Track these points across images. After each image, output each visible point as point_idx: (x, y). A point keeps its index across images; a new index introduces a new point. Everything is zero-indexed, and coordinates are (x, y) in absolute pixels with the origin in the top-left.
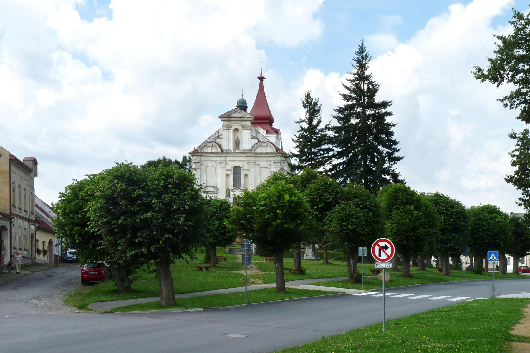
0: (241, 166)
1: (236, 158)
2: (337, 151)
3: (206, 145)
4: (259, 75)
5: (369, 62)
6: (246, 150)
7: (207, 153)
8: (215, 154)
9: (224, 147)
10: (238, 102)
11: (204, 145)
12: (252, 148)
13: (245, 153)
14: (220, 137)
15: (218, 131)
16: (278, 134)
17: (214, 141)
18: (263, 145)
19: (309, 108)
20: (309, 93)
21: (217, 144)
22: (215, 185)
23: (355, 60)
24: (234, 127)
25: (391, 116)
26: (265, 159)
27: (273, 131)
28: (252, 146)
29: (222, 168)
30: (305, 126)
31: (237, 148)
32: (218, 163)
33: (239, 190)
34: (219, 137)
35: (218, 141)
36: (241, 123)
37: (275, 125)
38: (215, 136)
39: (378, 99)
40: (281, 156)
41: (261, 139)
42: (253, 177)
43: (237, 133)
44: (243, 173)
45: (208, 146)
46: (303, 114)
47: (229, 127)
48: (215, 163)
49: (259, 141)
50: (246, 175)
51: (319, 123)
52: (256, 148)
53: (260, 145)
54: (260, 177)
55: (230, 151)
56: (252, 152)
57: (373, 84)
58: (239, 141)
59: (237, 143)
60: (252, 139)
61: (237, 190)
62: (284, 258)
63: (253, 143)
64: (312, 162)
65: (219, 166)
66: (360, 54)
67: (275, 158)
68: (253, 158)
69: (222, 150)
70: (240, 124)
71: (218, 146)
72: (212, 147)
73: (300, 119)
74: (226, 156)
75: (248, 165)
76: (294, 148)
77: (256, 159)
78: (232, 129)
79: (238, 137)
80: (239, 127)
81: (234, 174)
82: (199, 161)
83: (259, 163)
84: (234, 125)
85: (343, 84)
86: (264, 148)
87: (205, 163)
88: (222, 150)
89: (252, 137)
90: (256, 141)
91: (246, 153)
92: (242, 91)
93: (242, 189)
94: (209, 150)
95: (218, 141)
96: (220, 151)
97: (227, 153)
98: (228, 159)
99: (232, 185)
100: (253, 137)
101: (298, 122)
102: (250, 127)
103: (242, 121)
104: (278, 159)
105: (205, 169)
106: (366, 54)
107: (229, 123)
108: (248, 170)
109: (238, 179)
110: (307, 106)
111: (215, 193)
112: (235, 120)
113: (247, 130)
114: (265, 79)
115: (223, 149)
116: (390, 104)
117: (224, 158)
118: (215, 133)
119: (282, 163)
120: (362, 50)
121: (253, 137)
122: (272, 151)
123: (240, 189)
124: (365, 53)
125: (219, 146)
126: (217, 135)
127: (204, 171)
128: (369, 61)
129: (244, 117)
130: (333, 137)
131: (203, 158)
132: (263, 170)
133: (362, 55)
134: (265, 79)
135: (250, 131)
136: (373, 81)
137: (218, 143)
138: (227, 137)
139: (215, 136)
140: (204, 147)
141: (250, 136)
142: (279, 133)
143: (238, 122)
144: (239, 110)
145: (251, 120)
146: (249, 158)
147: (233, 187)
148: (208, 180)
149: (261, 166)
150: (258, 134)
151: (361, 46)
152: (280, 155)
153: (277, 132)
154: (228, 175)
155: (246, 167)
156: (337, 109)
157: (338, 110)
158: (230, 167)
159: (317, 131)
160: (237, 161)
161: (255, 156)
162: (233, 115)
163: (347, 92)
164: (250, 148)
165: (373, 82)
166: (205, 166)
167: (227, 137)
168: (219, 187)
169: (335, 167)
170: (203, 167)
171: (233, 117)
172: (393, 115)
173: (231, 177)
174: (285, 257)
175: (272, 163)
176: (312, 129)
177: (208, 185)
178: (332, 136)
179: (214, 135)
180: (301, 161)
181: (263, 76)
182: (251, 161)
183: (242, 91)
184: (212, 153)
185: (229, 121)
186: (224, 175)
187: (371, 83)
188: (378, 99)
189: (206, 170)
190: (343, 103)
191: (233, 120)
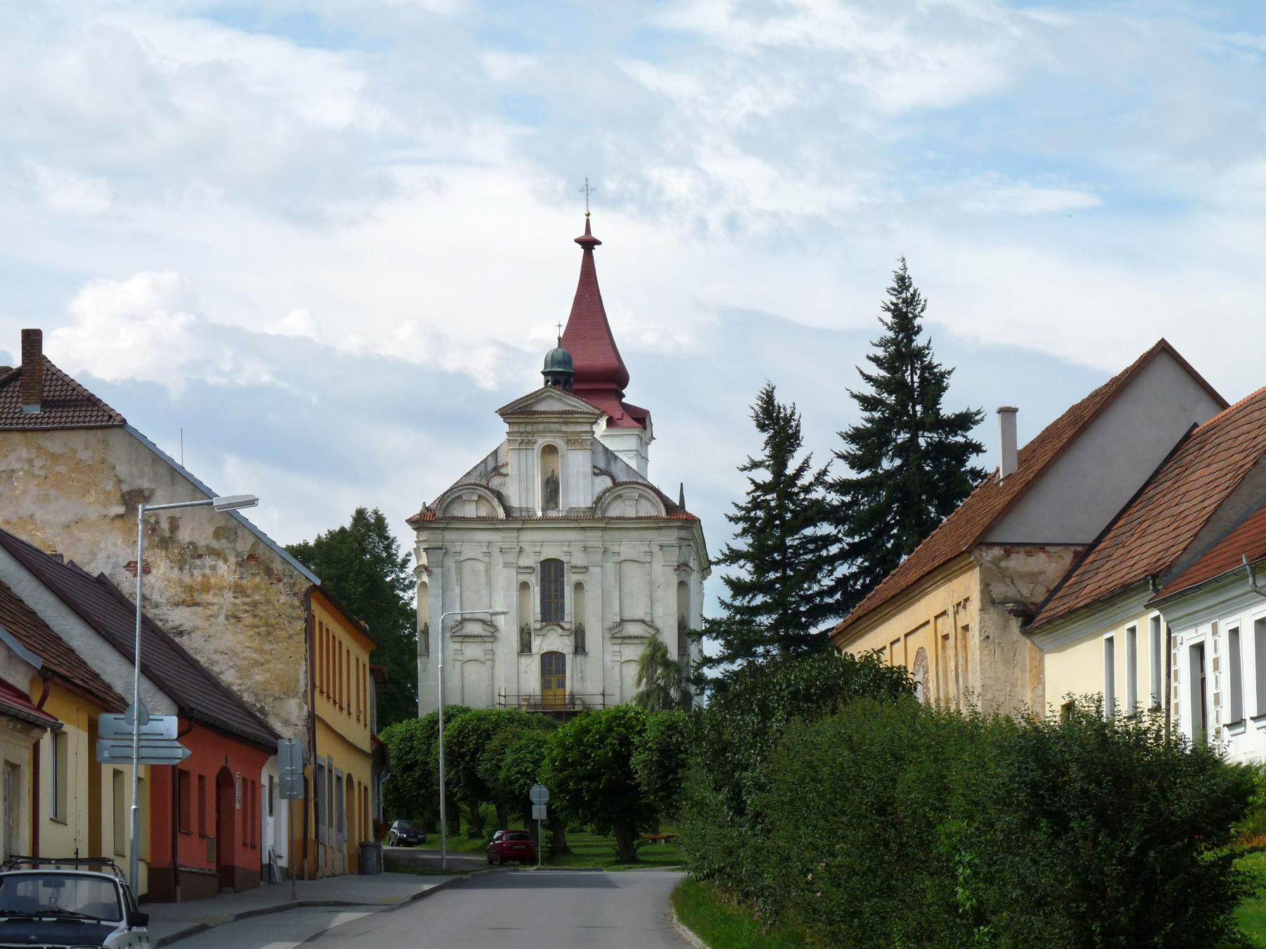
0: (564, 559)
1: (548, 535)
2: (848, 544)
3: (460, 497)
4: (581, 233)
5: (921, 314)
7: (464, 519)
8: (488, 523)
9: (514, 502)
10: (549, 359)
11: (451, 497)
12: (596, 503)
13: (576, 520)
14: (503, 470)
15: (495, 453)
16: (645, 428)
17: (484, 483)
18: (626, 492)
19: (774, 429)
20: (772, 392)
22: (648, 619)
23: (888, 309)
24: (542, 441)
25: (980, 454)
26: (635, 534)
27: (628, 420)
28: (595, 499)
29: (506, 565)
30: (765, 476)
33: (560, 631)
35: (495, 482)
36: (564, 428)
37: (631, 396)
39: (949, 406)
40: (680, 528)
41: (622, 478)
42: (600, 591)
43: (551, 459)
44: (570, 579)
45: (464, 498)
46: (757, 444)
48: (485, 549)
50: (579, 586)
51: (801, 470)
52: (609, 503)
53: (620, 496)
54: (620, 590)
55: (531, 514)
57: (935, 370)
58: (556, 483)
59: (552, 488)
60: (595, 477)
61: (552, 632)
62: (103, 856)
64: (784, 572)
66: (900, 293)
67: (663, 532)
68: (599, 533)
69: (507, 510)
70: (559, 432)
71: (496, 500)
73: (752, 461)
74: (519, 529)
75: (583, 555)
76: (737, 536)
77: (608, 535)
78: (538, 447)
79: (553, 471)
80: (559, 443)
82: (440, 544)
83: (616, 549)
84: (544, 437)
85: (861, 372)
86: (630, 502)
87: (458, 549)
88: (507, 510)
89: (597, 471)
90: (608, 482)
91: (576, 520)
93: (566, 626)
94: (470, 511)
95: (495, 482)
96: (501, 513)
97: (524, 521)
98: (526, 536)
99: (539, 617)
100: (598, 472)
101: (745, 469)
102: (589, 442)
103: (566, 423)
104: (671, 537)
105: (457, 568)
106: (913, 295)
107: (529, 428)
108: (585, 569)
109: (556, 597)
110: (768, 425)
111: (486, 639)
113: (581, 452)
114: (599, 243)
116: (977, 418)
117: (514, 534)
118: (486, 459)
119: (683, 547)
120: (903, 282)
121: (598, 472)
122: (654, 513)
123: (562, 628)
124: (911, 290)
125: (500, 497)
126: (491, 465)
127: (453, 576)
128: (922, 310)
129: (572, 413)
130: (837, 506)
131: (449, 535)
132: (629, 569)
133: (904, 295)
134: (599, 243)
135: (588, 454)
136: (935, 362)
137: (494, 488)
138: (523, 470)
140: (453, 501)
141: (589, 469)
142: (648, 423)
143: (553, 427)
144: (556, 392)
146: (589, 533)
147: (542, 621)
148: (464, 600)
149: (623, 557)
150: (612, 462)
151: (901, 272)
152: (678, 524)
153: (640, 418)
154: (524, 586)
155: (578, 559)
156: (846, 433)
157: (849, 436)
158: (529, 560)
159: (796, 490)
160: (551, 545)
161: (604, 529)
162: (541, 407)
163: (870, 390)
164: (590, 505)
165: (935, 367)
166: (457, 558)
167: (523, 470)
169: (842, 583)
170: (450, 563)
171: (544, 413)
172: (985, 452)
173: (536, 591)
174: (100, 852)
175: (656, 549)
176: (782, 484)
177: (467, 616)
178: (835, 503)
179: (483, 465)
180: (760, 570)
181: (595, 234)
182: (595, 544)
184: (479, 519)
185: (527, 423)
186: (515, 586)
187: (930, 367)
188: (949, 406)
189: (459, 571)
190: (858, 418)
191: (539, 420)
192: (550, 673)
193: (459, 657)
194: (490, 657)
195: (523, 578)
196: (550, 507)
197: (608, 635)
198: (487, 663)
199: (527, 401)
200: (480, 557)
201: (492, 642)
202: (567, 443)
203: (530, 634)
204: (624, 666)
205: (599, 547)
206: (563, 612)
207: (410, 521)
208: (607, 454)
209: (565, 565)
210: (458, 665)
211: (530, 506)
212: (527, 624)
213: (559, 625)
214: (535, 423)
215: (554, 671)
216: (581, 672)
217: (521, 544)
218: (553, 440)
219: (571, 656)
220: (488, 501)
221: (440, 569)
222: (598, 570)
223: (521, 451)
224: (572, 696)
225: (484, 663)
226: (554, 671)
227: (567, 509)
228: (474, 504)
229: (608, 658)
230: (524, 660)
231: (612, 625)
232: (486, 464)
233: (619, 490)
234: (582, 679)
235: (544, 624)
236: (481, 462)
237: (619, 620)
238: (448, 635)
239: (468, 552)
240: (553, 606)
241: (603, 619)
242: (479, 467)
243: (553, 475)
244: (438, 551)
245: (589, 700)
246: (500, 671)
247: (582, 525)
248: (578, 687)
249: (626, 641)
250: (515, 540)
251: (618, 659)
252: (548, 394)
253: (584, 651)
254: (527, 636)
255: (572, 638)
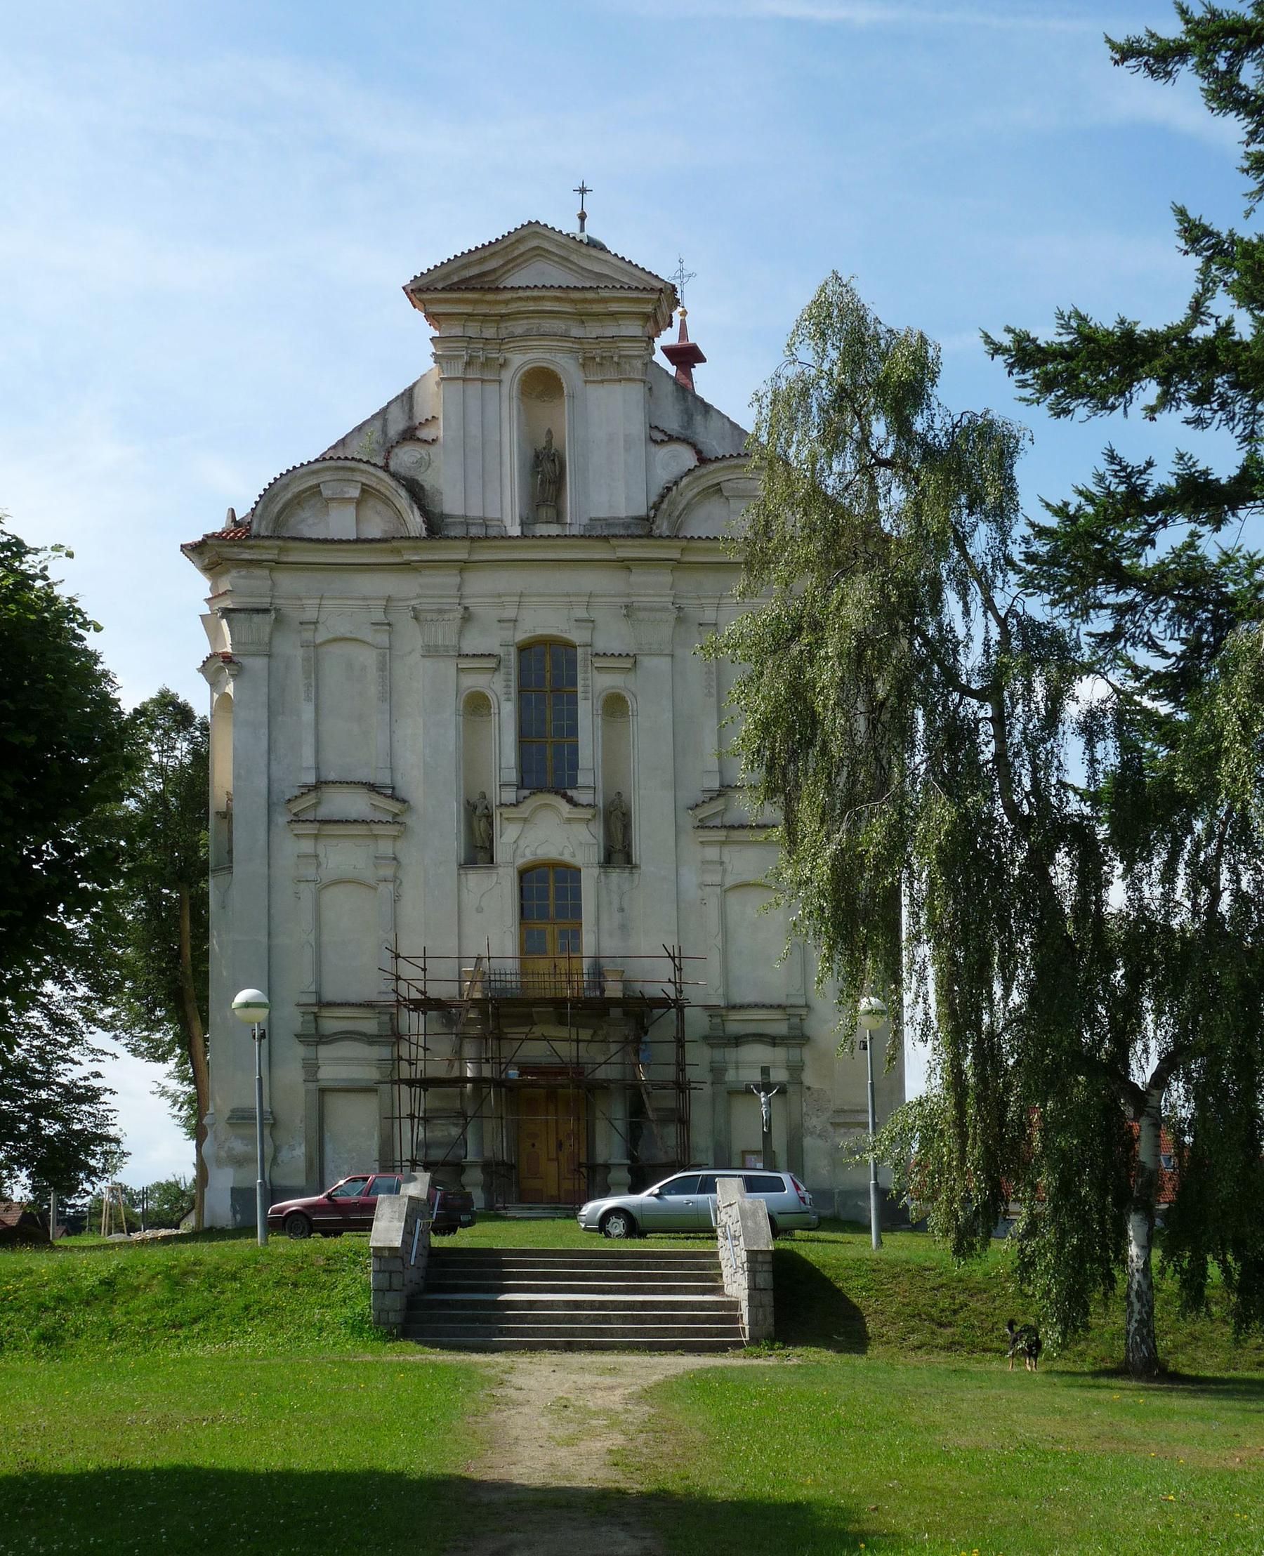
0: (576, 636)
3: (315, 490)
6: (608, 522)
9: (451, 503)
12: (656, 507)
14: (424, 434)
15: (408, 397)
17: (381, 462)
21: (394, 476)
22: (383, 778)
24: (520, 361)
28: (654, 498)
29: (431, 652)
31: (545, 513)
32: (405, 623)
33: (565, 807)
34: (409, 435)
35: (405, 457)
38: (384, 431)
45: (327, 493)
47: (487, 363)
48: (379, 616)
49: (703, 460)
50: (615, 706)
56: (657, 532)
60: (654, 448)
63: (663, 476)
65: (411, 638)
68: (665, 578)
70: (565, 337)
71: (403, 493)
72: (359, 503)
74: (464, 566)
78: (510, 379)
79: (549, 432)
80: (566, 366)
81: (527, 691)
82: (264, 602)
87: (310, 614)
90: (688, 458)
92: (583, 191)
93: (583, 797)
94: (341, 522)
96: (416, 524)
98: (481, 585)
99: (512, 776)
100: (659, 437)
105: (306, 659)
107: (490, 332)
108: (631, 661)
111: (378, 830)
112: (532, 306)
115: (443, 516)
117: (449, 579)
121: (659, 437)
125: (416, 491)
126: (397, 425)
131: (288, 582)
135: (635, 392)
137: (403, 471)
139: (384, 431)
141: (638, 429)
145: (649, 308)
146: (639, 577)
150: (698, 419)
154: (476, 705)
161: (677, 565)
162: (518, 279)
164: (642, 512)
166: (308, 635)
168: (413, 783)
170: (291, 648)
173: (506, 712)
179: (378, 424)
183: (583, 191)
186: (450, 713)
189: (314, 669)
191: (513, 307)
192: (543, 915)
193: (310, 872)
194: (388, 872)
195: (474, 682)
196: (544, 516)
197: (689, 820)
198: (382, 886)
199: (482, 260)
200: (367, 634)
201: (395, 838)
202: (584, 366)
203: (489, 818)
204: (733, 898)
205: (665, 609)
206: (574, 766)
207: (195, 550)
208: (685, 399)
209: (580, 651)
210: (307, 891)
211: (493, 513)
212: (483, 796)
213: (564, 796)
214: (502, 316)
215: (552, 910)
216: (622, 910)
217: (467, 602)
218: (547, 356)
219: (595, 871)
220: (387, 501)
221: (266, 660)
222: (663, 664)
223: (470, 385)
224: (598, 972)
225: (375, 889)
226: (552, 910)
227: (585, 521)
228: (351, 509)
229: (690, 878)
230: (475, 880)
231: (700, 797)
232: (385, 420)
233: (713, 474)
234: (624, 929)
235: (526, 792)
236: (373, 417)
237: (716, 785)
238: (281, 819)
239: (337, 622)
240: (549, 752)
241: (676, 785)
242: (368, 430)
243: (549, 442)
244: (257, 618)
245: (636, 970)
246: (412, 910)
247: (622, 553)
248: (611, 946)
249: (736, 835)
250: (454, 592)
251: (716, 879)
252: (534, 243)
253: (628, 859)
254: (483, 824)
255: (598, 829)
